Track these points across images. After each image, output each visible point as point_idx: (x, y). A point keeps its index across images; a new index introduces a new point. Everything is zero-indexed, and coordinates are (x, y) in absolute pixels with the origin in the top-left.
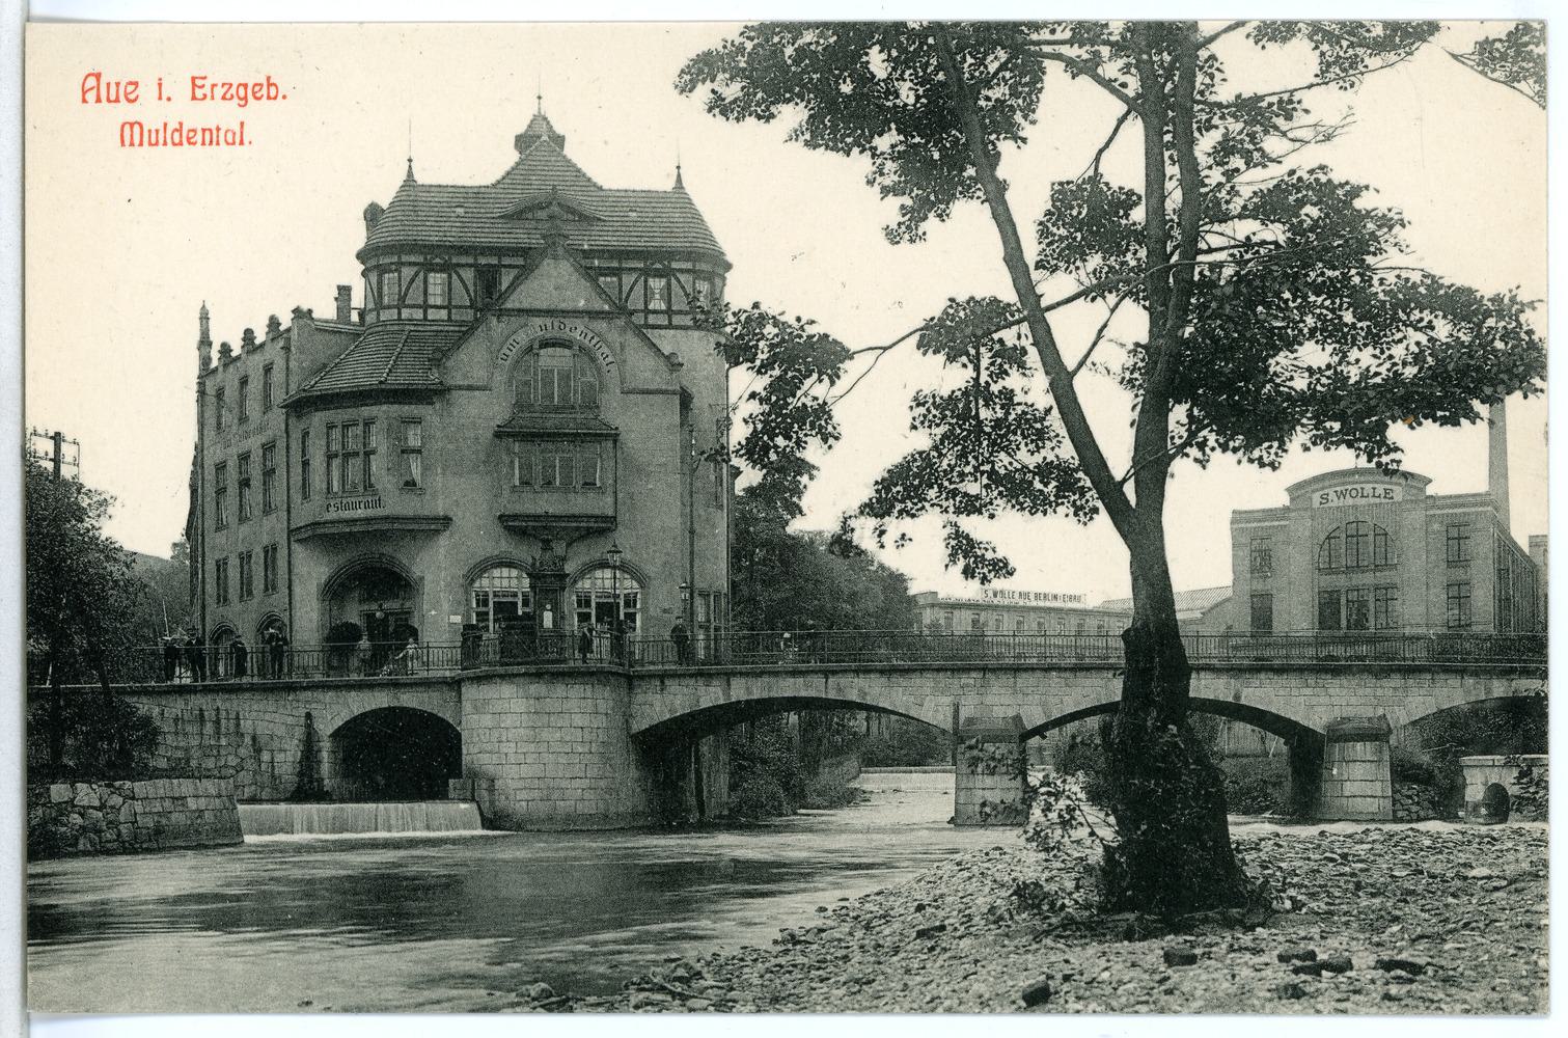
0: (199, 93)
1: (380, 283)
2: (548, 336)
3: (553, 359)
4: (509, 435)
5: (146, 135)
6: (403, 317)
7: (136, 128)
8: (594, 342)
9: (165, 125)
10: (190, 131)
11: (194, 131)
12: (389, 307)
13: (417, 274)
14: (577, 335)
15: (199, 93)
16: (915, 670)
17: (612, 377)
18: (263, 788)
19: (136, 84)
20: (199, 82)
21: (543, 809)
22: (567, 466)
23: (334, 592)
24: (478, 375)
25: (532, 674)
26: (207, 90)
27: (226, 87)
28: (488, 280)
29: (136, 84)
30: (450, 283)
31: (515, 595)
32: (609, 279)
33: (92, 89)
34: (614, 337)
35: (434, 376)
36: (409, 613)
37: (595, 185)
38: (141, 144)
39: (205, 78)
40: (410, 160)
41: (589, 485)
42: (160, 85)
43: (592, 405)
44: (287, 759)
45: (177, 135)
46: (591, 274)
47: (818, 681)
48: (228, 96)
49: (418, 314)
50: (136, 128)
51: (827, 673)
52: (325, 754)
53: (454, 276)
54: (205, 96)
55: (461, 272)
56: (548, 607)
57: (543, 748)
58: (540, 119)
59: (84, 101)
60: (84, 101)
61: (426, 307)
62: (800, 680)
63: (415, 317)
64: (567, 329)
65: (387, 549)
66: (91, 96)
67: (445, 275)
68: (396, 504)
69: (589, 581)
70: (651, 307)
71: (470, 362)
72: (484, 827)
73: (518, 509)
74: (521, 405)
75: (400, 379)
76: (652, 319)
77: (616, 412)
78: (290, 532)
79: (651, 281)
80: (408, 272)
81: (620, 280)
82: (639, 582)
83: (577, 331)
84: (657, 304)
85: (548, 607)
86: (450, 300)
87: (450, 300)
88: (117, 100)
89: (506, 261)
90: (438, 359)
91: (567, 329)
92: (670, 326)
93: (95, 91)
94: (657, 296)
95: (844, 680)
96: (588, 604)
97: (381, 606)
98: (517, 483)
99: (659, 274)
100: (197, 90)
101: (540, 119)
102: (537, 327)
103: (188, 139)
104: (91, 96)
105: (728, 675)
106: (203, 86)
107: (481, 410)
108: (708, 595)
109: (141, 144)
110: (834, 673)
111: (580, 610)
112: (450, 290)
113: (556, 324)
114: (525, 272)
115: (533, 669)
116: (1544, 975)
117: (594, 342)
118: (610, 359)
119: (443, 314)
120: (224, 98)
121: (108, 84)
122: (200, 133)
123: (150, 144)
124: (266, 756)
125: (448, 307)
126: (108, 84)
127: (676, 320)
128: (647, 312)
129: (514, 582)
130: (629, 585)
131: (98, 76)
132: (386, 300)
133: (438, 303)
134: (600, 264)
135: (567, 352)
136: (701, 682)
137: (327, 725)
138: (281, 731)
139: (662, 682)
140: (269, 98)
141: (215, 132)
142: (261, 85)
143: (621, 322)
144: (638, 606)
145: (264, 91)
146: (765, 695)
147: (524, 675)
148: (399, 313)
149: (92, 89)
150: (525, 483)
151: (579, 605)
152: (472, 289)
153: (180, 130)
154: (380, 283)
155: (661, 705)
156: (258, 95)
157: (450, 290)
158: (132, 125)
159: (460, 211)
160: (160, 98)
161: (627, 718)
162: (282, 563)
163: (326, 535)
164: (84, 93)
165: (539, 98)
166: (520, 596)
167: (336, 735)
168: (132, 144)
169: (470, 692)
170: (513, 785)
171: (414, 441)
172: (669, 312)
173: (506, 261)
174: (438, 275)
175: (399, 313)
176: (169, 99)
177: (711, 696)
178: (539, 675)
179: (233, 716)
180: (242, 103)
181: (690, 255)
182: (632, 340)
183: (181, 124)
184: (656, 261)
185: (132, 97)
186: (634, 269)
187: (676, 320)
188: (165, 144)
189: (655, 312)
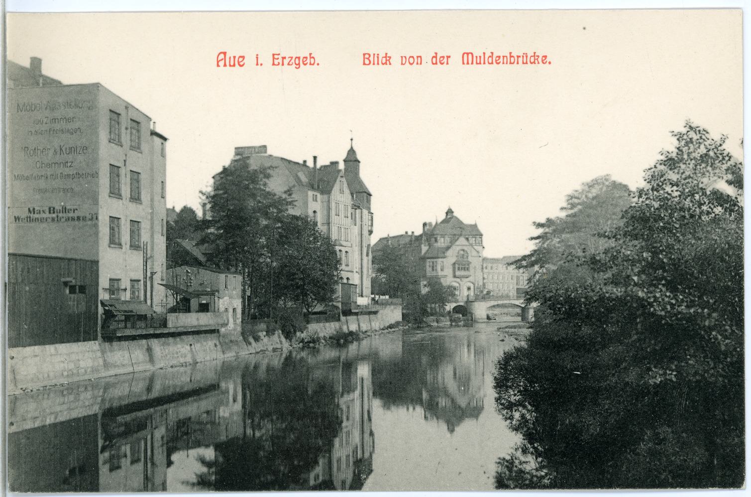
0: (276, 62)
7: (470, 56)
9: (484, 53)
10: (497, 57)
15: (276, 62)
19: (243, 57)
20: (276, 57)
26: (280, 60)
27: (290, 59)
29: (243, 57)
33: (222, 60)
38: (472, 63)
39: (279, 54)
42: (257, 58)
48: (291, 63)
50: (470, 56)
54: (279, 63)
59: (218, 66)
60: (218, 66)
66: (222, 63)
88: (234, 65)
93: (223, 61)
100: (275, 60)
104: (222, 63)
106: (278, 59)
109: (472, 63)
115: (8, 132)
116: (740, 166)
120: (289, 64)
121: (230, 58)
122: (502, 58)
123: (477, 63)
126: (230, 58)
131: (225, 53)
140: (310, 64)
142: (306, 58)
145: (308, 61)
149: (222, 60)
153: (491, 57)
156: (305, 63)
158: (468, 54)
160: (257, 64)
164: (218, 62)
165: (352, 140)
168: (468, 63)
180: (298, 66)
185: (241, 64)
188: (484, 63)
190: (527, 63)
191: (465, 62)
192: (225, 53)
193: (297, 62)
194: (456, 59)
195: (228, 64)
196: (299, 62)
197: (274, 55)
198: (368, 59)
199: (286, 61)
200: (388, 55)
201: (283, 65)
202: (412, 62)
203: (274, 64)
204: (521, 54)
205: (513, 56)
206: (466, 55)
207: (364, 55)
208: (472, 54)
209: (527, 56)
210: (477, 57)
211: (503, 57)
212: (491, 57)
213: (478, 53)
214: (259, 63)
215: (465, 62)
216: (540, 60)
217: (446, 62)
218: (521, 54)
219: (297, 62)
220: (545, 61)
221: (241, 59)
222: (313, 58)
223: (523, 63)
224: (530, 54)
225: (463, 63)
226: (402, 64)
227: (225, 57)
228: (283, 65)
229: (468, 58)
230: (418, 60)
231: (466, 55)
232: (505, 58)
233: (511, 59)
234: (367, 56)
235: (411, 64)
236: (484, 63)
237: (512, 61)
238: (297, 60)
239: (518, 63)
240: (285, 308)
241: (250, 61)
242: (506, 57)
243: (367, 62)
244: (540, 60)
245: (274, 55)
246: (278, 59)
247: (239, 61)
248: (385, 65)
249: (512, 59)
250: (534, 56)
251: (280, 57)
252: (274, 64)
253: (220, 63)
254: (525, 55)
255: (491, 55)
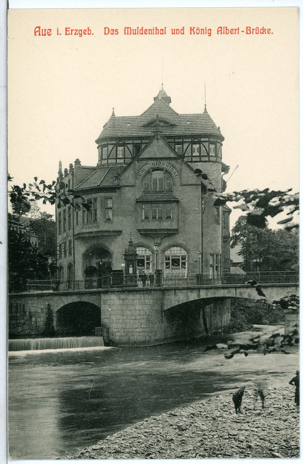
0: (68, 33)
1: (102, 151)
2: (154, 167)
3: (157, 175)
4: (140, 202)
5: (132, 31)
6: (109, 163)
7: (129, 29)
8: (171, 168)
9: (138, 28)
10: (145, 30)
11: (147, 30)
12: (105, 159)
13: (114, 147)
14: (165, 166)
15: (68, 33)
16: (269, 287)
17: (177, 180)
18: (32, 330)
19: (50, 30)
21: (124, 339)
22: (161, 212)
23: (86, 256)
24: (131, 181)
25: (121, 291)
26: (70, 32)
27: (76, 31)
28: (138, 149)
30: (125, 149)
31: (144, 256)
32: (179, 146)
33: (37, 31)
34: (178, 166)
35: (116, 182)
36: (110, 263)
37: (176, 113)
38: (131, 34)
40: (113, 109)
41: (169, 217)
42: (58, 30)
43: (170, 191)
44: (41, 320)
45: (141, 31)
46: (169, 144)
47: (233, 291)
49: (114, 161)
50: (129, 29)
51: (236, 288)
52: (54, 318)
53: (126, 147)
54: (69, 33)
55: (128, 146)
56: (131, 266)
57: (125, 317)
58: (162, 92)
59: (218, 34)
61: (116, 158)
62: (226, 291)
63: (113, 162)
64: (162, 164)
65: (101, 241)
66: (220, 32)
67: (123, 147)
68: (105, 227)
69: (169, 251)
70: (194, 155)
71: (128, 177)
72: (105, 345)
73: (146, 227)
74: (146, 192)
75: (106, 184)
76: (194, 159)
77: (178, 193)
78: (74, 236)
79: (194, 146)
80: (110, 147)
81: (183, 146)
82: (187, 251)
83: (165, 164)
84: (196, 154)
85: (131, 266)
86: (125, 156)
87: (125, 156)
89: (143, 141)
90: (117, 177)
91: (162, 164)
92: (200, 161)
93: (38, 32)
94: (196, 151)
95: (242, 290)
96: (169, 259)
97: (101, 260)
98: (143, 218)
99: (195, 143)
101: (162, 92)
102: (151, 164)
103: (145, 32)
104: (220, 32)
105: (199, 289)
107: (130, 195)
108: (214, 255)
109: (131, 34)
110: (238, 288)
111: (166, 261)
112: (124, 152)
113: (158, 163)
114: (147, 145)
117: (171, 168)
118: (177, 174)
119: (122, 161)
120: (75, 34)
122: (148, 30)
124: (34, 319)
125: (124, 158)
127: (203, 159)
128: (192, 156)
129: (144, 252)
130: (184, 253)
131: (39, 27)
132: (104, 157)
133: (121, 157)
134: (173, 140)
135: (162, 172)
136: (189, 291)
137: (55, 309)
138: (39, 311)
139: (175, 292)
140: (88, 34)
141: (152, 30)
142: (86, 30)
143: (179, 161)
144: (186, 260)
145: (87, 32)
146: (213, 296)
147: (118, 291)
148: (108, 161)
150: (146, 218)
151: (166, 260)
152: (132, 151)
153: (142, 30)
154: (102, 151)
155: (175, 300)
157: (124, 152)
158: (128, 28)
159: (129, 125)
160: (58, 34)
161: (162, 305)
162: (72, 244)
163: (84, 237)
164: (35, 33)
165: (162, 84)
166: (146, 257)
167: (59, 311)
168: (128, 34)
169: (103, 297)
170: (115, 330)
171: (110, 205)
172: (200, 156)
173: (143, 141)
174: (121, 147)
175: (108, 161)
176: (93, 34)
177: (211, 294)
178: (123, 292)
179: (22, 305)
180: (80, 35)
181: (205, 136)
182: (184, 167)
183: (142, 28)
184: (196, 139)
185: (49, 34)
186: (188, 142)
187: (203, 159)
188: (138, 34)
189: (195, 156)
190: (258, 33)
191: (126, 32)
192: (39, 27)
193: (80, 33)
194: (121, 31)
195: (41, 34)
196: (81, 33)
197: (66, 28)
198: (249, 30)
199: (74, 32)
200: (264, 28)
201: (72, 34)
202: (198, 32)
203: (66, 34)
204: (255, 28)
205: (228, 29)
206: (127, 29)
207: (247, 28)
208: (130, 28)
209: (258, 29)
210: (133, 30)
211: (149, 30)
212: (142, 30)
213: (134, 27)
214: (59, 34)
215: (126, 32)
216: (266, 31)
217: (234, 33)
218: (255, 28)
219: (80, 33)
220: (146, 33)
221: (49, 31)
222: (90, 30)
223: (256, 33)
224: (260, 28)
225: (125, 34)
226: (105, 34)
227: (221, 29)
228: (72, 34)
229: (128, 31)
230: (182, 31)
231: (127, 29)
232: (150, 31)
233: (143, 31)
234: (249, 28)
235: (198, 34)
236: (138, 34)
237: (227, 32)
238: (80, 31)
239: (253, 33)
240: (47, 270)
241: (54, 32)
242: (203, 29)
243: (249, 32)
244: (266, 31)
245: (66, 28)
246: (69, 31)
247: (48, 32)
248: (262, 34)
249: (227, 31)
250: (263, 29)
251: (70, 30)
252: (66, 34)
253: (219, 33)
254: (257, 29)
255: (142, 28)
